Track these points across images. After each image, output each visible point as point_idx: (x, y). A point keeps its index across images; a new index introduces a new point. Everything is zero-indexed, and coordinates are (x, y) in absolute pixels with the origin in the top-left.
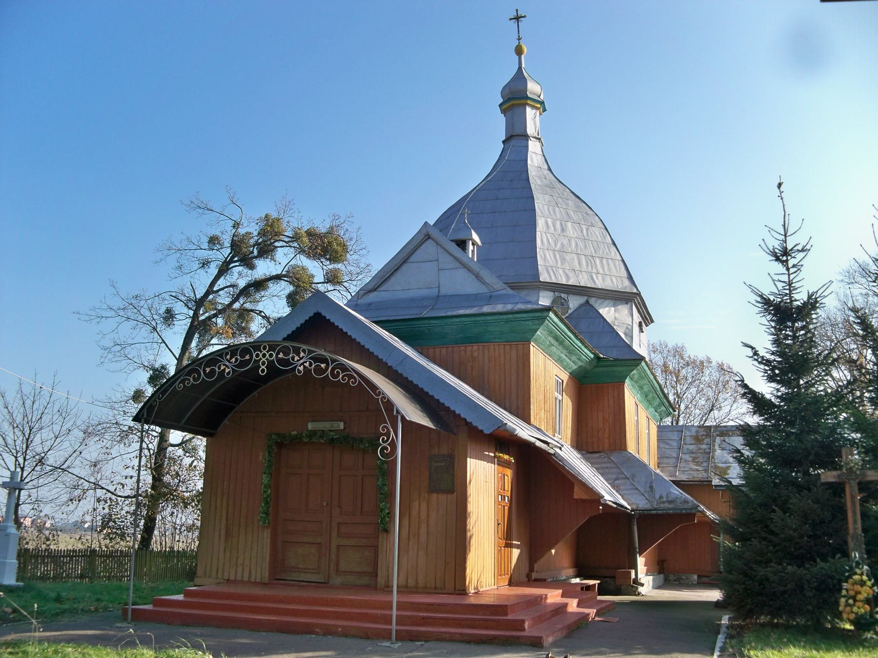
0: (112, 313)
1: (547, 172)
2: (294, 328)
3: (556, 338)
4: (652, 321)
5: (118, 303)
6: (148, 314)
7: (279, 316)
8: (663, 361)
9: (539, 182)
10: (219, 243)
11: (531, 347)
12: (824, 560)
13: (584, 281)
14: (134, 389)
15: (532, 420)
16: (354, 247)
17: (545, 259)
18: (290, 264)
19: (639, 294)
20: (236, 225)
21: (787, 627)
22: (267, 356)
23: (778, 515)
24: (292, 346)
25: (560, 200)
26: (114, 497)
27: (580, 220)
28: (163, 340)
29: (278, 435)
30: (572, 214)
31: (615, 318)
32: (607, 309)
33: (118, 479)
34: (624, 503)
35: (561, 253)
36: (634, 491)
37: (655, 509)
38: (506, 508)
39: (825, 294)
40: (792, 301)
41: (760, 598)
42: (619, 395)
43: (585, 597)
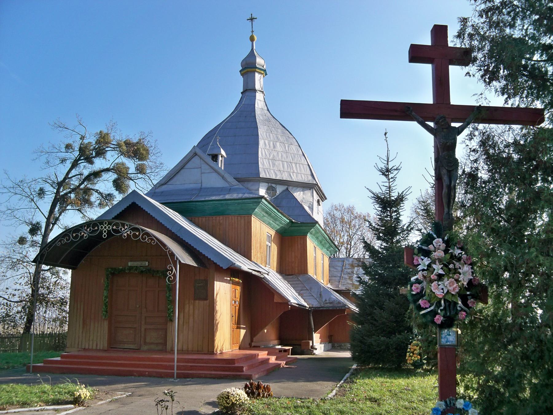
0: (6, 190)
1: (267, 112)
2: (121, 211)
3: (267, 213)
4: (326, 199)
5: (9, 184)
6: (27, 190)
7: (108, 193)
8: (341, 215)
9: (261, 118)
10: (72, 148)
11: (252, 218)
12: (400, 334)
13: (285, 177)
14: (19, 236)
15: (252, 258)
16: (153, 151)
17: (263, 164)
18: (115, 162)
19: (317, 185)
20: (82, 138)
21: (382, 369)
22: (107, 228)
23: (377, 311)
24: (121, 223)
25: (273, 128)
26: (9, 302)
27: (285, 141)
28: (37, 207)
29: (112, 268)
30: (280, 137)
31: (303, 198)
32: (299, 192)
33: (9, 291)
34: (306, 304)
35: (273, 161)
36: (311, 297)
37: (322, 307)
38: (237, 308)
39: (407, 193)
40: (390, 197)
41: (368, 354)
42: (304, 243)
43: (279, 355)
